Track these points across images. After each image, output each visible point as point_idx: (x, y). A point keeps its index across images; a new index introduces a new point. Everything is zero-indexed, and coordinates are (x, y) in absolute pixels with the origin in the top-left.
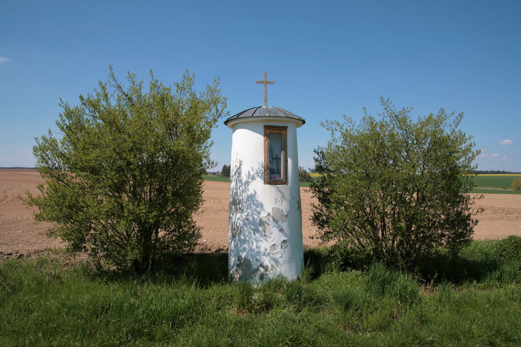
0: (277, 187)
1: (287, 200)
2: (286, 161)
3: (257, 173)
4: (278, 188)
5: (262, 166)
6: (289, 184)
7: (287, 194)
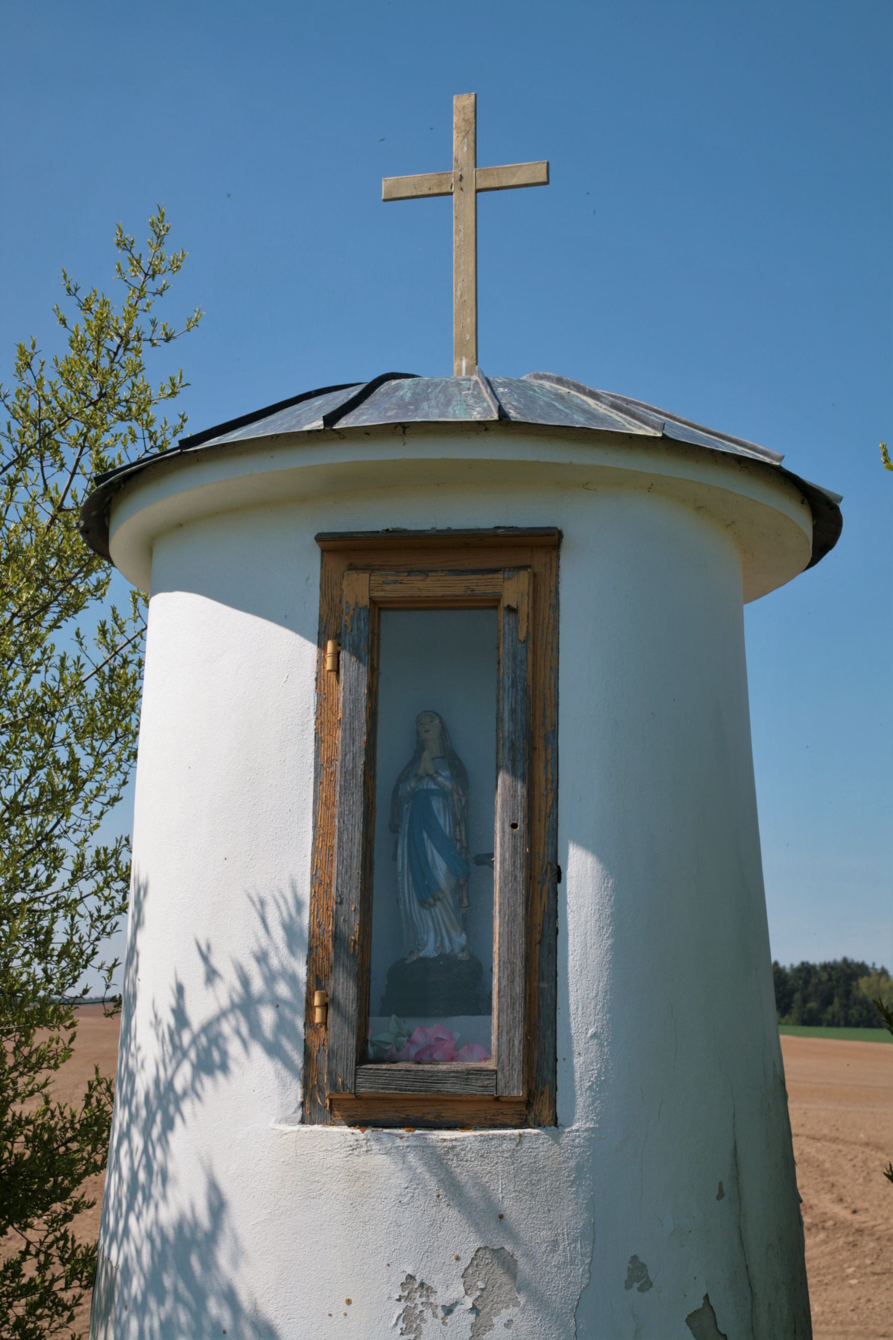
0: (425, 1149)
1: (539, 1301)
2: (542, 878)
3: (246, 1005)
4: (438, 1161)
5: (289, 929)
6: (580, 1123)
7: (550, 1231)
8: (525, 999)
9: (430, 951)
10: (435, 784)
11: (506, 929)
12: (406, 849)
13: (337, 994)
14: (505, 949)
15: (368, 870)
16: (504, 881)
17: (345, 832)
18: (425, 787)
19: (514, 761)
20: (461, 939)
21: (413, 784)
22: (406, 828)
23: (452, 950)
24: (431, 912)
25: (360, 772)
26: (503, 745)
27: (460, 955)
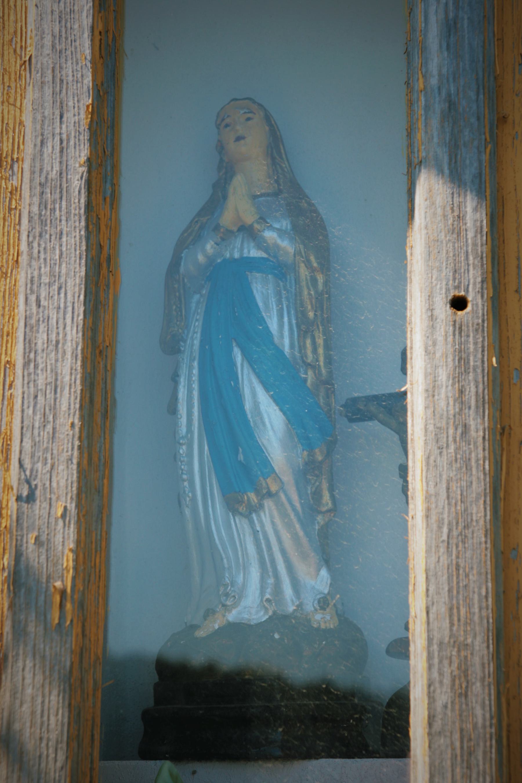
8: (499, 741)
9: (249, 607)
10: (259, 247)
11: (444, 560)
12: (196, 386)
13: (17, 726)
14: (444, 610)
15: (98, 418)
16: (437, 439)
17: (42, 327)
18: (236, 255)
19: (454, 148)
20: (319, 581)
21: (210, 247)
22: (197, 342)
23: (300, 606)
24: (252, 523)
25: (77, 181)
26: (427, 108)
27: (318, 617)
